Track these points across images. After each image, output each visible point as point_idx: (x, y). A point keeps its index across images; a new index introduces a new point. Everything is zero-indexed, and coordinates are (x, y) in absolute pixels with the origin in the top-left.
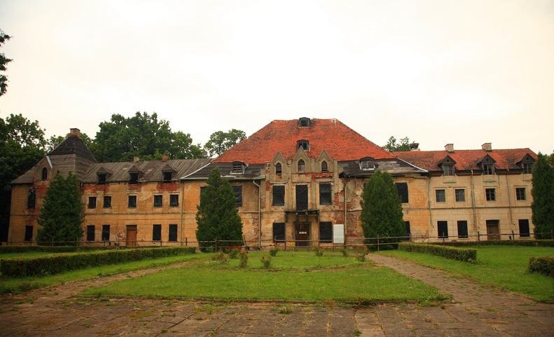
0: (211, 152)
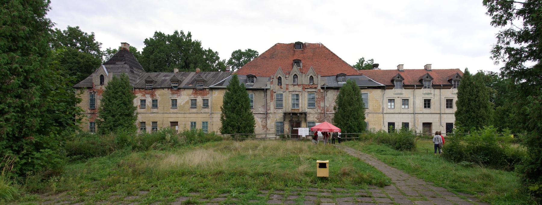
0: (233, 68)
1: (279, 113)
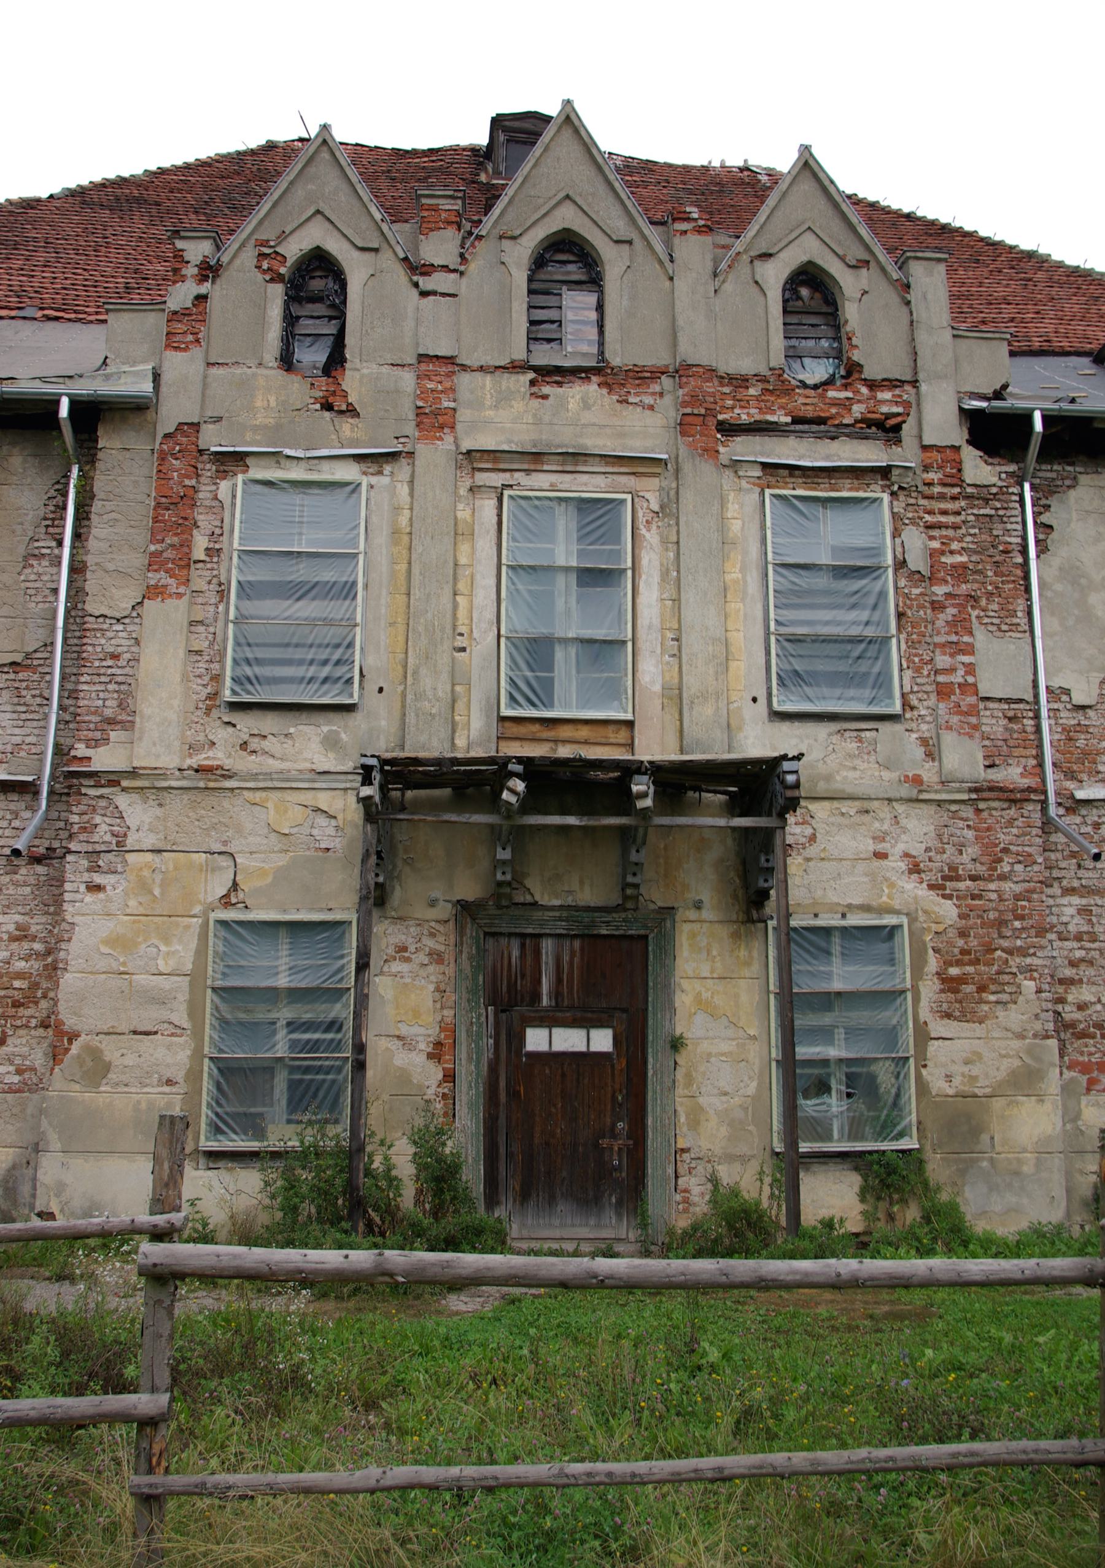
1: (280, 784)
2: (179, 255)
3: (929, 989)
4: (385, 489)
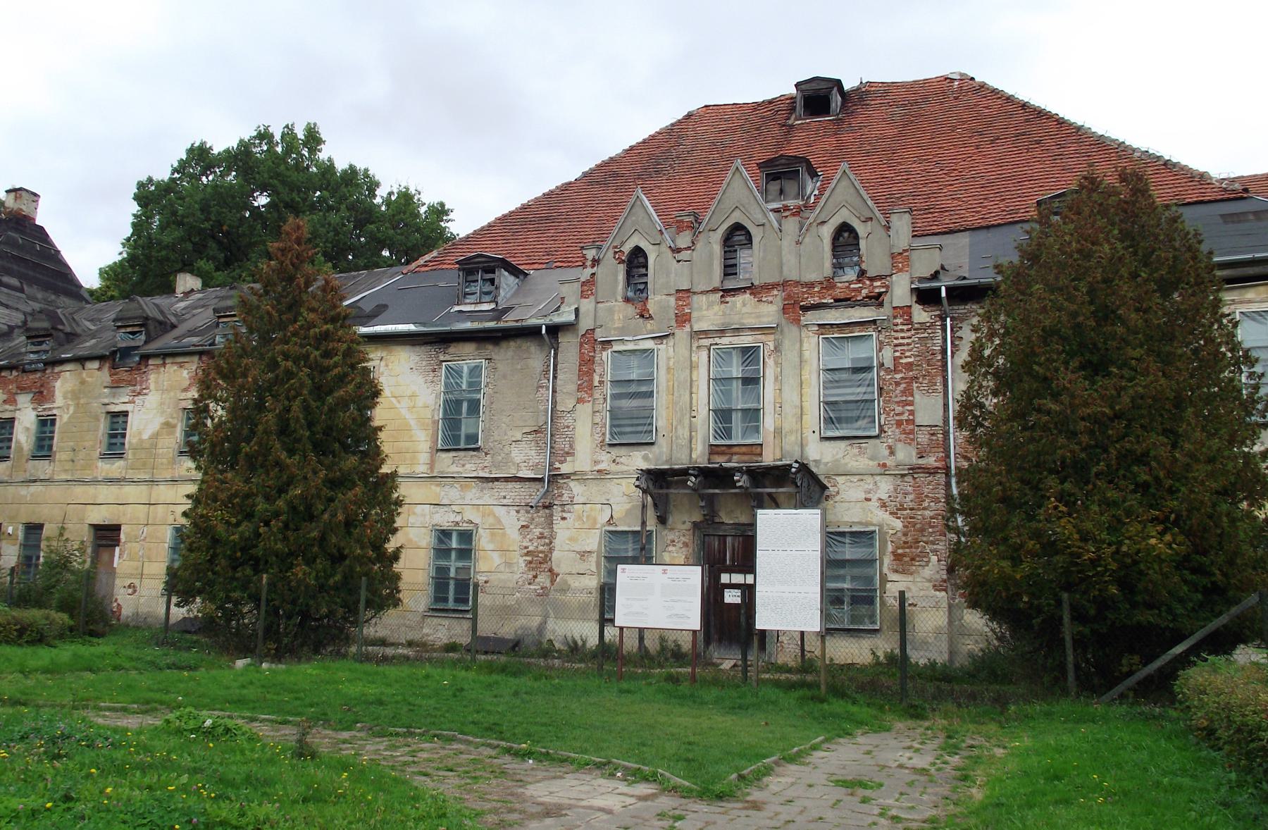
2: (584, 256)
3: (887, 560)
4: (664, 351)
